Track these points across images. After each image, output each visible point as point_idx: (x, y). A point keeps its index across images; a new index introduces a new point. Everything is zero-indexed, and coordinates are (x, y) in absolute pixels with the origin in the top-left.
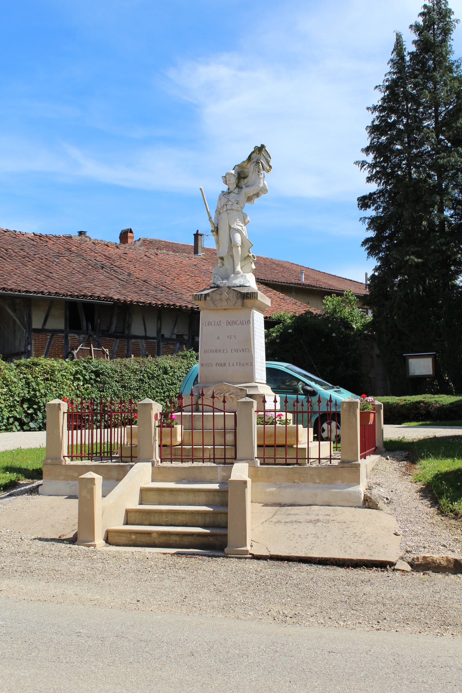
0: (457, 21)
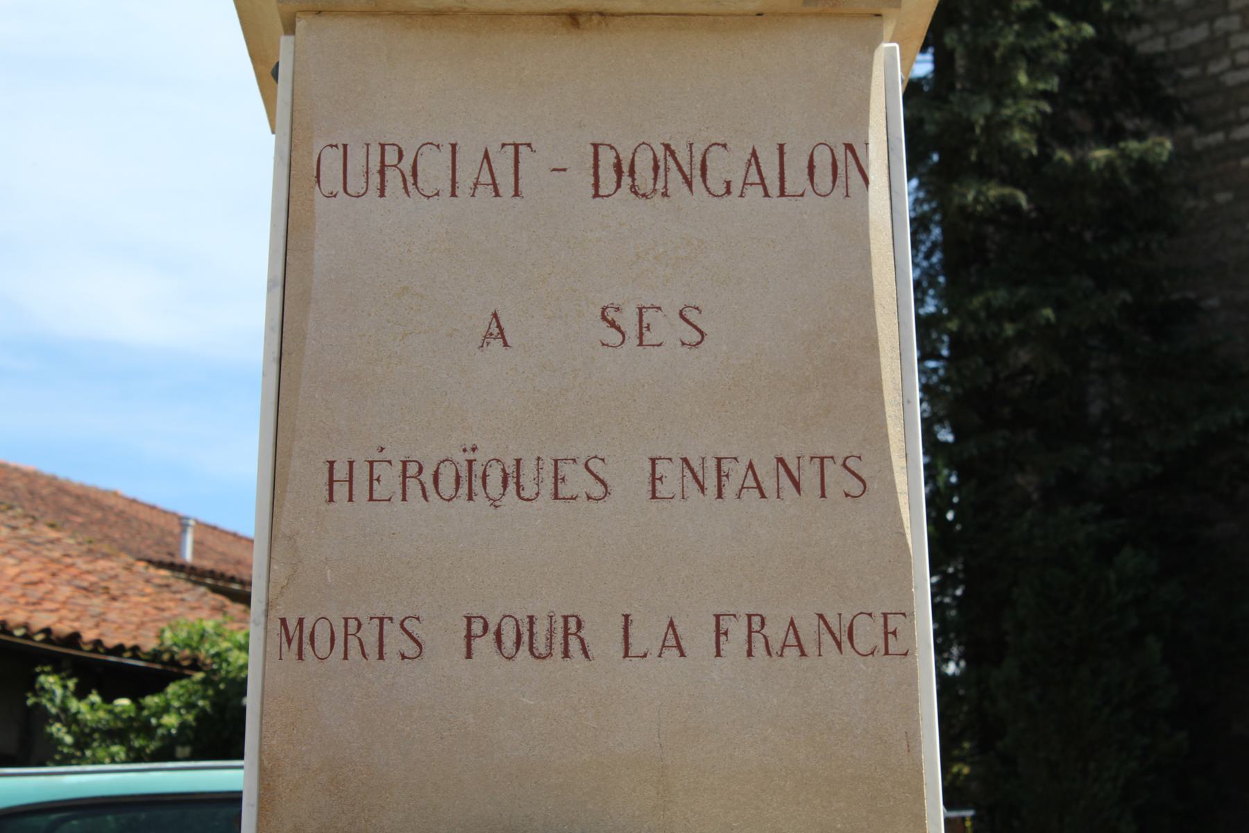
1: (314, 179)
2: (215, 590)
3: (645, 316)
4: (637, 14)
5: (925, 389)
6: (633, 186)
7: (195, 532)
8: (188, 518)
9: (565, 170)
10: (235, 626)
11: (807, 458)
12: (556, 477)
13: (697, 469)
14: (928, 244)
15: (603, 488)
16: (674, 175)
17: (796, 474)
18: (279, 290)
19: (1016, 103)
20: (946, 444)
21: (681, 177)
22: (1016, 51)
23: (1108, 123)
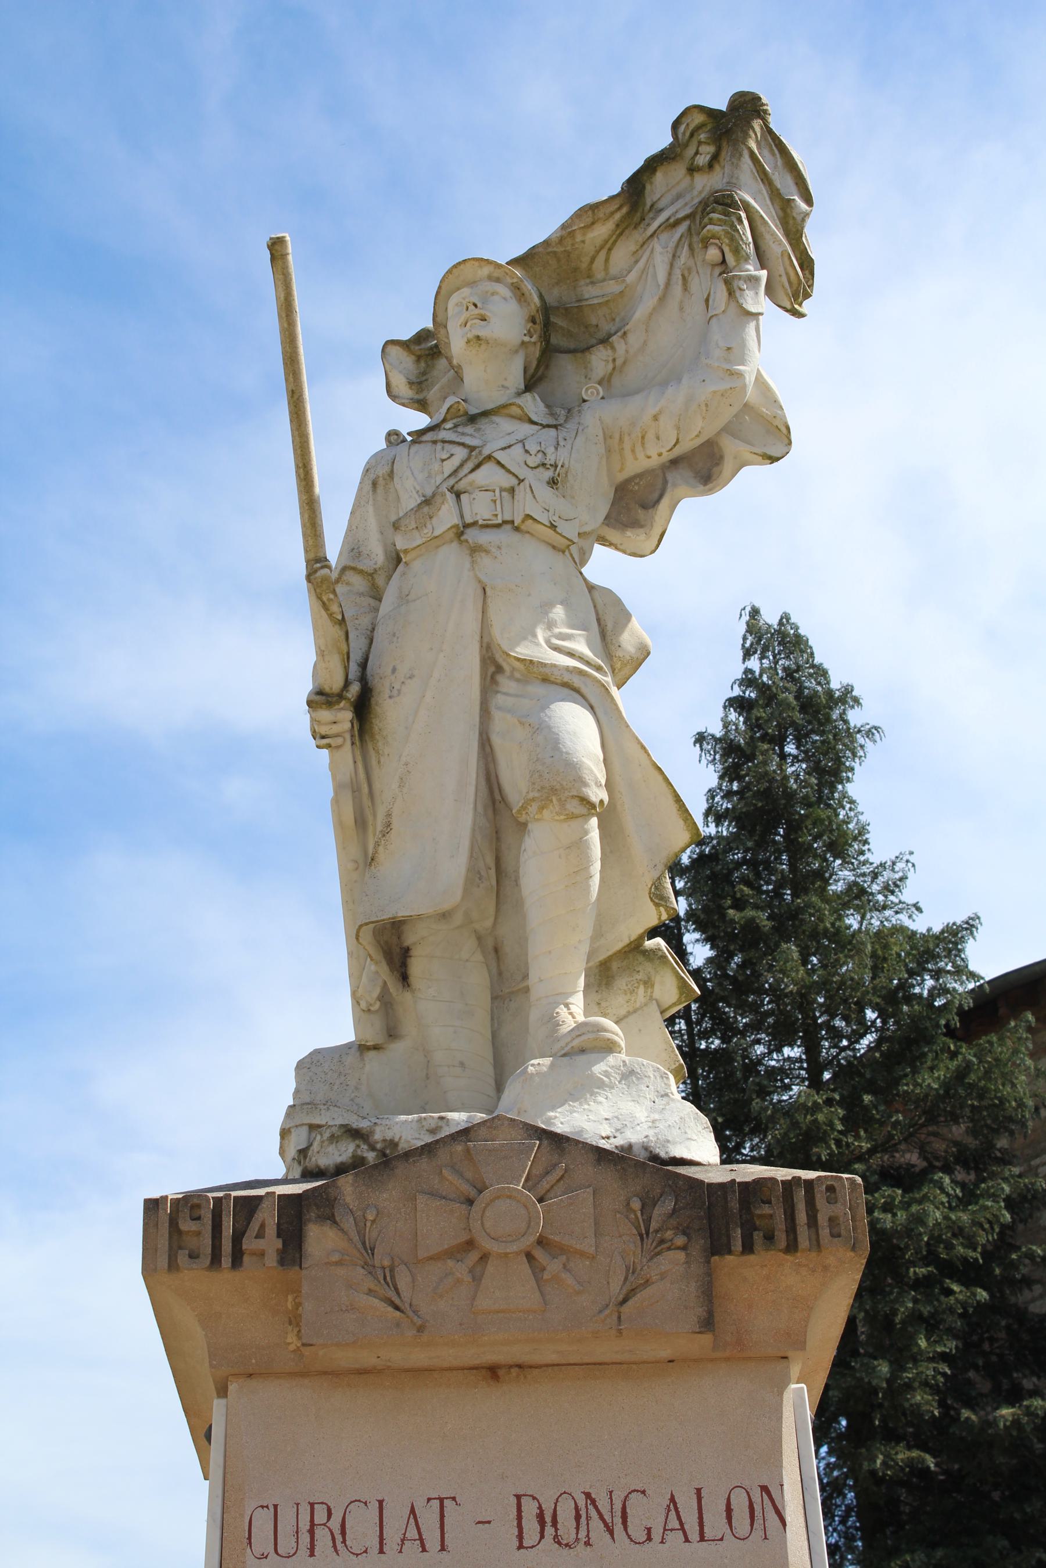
0: (871, 733)
1: (246, 1541)
4: (554, 1365)
6: (556, 1536)
9: (489, 1522)
16: (596, 1524)
19: (916, 1366)
21: (602, 1525)
22: (916, 1318)
23: (1006, 1384)
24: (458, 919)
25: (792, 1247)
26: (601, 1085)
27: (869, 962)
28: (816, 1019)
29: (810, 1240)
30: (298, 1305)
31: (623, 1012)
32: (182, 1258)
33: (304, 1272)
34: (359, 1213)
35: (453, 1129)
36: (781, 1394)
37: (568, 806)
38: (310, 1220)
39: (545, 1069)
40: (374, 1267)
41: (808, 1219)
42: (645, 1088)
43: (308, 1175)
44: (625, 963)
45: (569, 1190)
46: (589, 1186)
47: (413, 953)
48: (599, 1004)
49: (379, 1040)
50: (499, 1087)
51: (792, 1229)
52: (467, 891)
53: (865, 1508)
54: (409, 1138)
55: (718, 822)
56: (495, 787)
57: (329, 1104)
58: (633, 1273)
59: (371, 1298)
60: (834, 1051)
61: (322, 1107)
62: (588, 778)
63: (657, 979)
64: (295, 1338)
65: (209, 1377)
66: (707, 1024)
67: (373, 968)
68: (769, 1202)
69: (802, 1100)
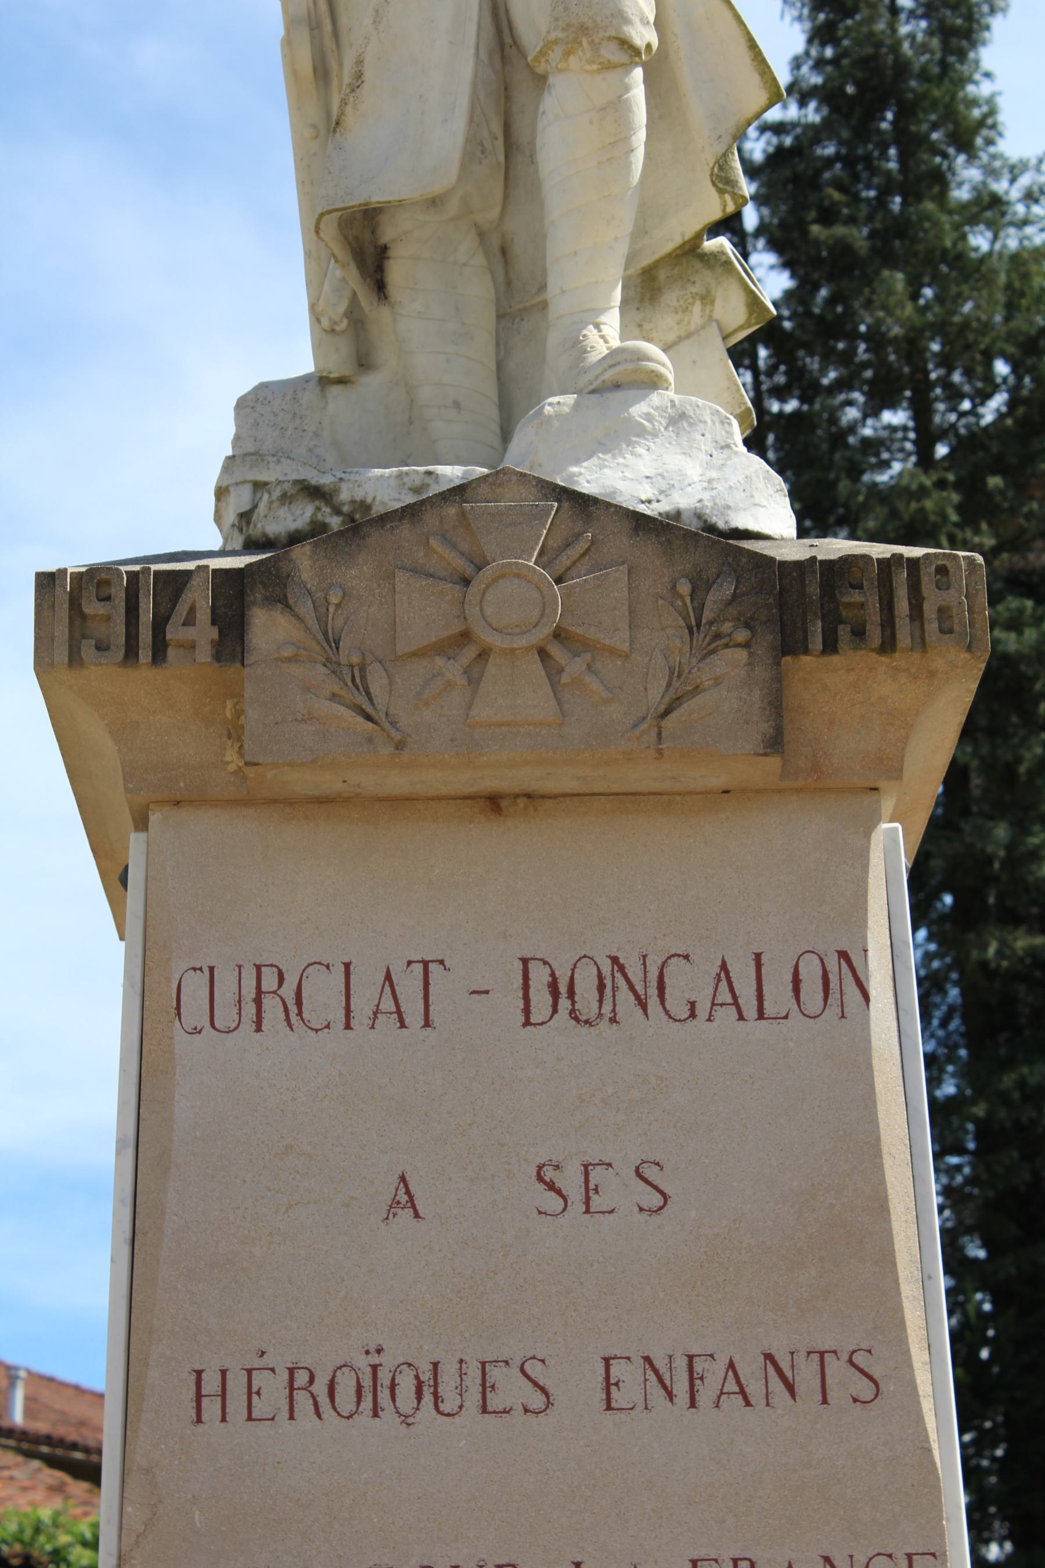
1: (173, 1011)
2: (53, 1462)
3: (592, 1175)
5: (946, 1192)
6: (573, 1011)
7: (27, 1383)
8: (17, 1368)
9: (487, 992)
10: (78, 1511)
11: (803, 1354)
12: (483, 1385)
13: (663, 1369)
14: (944, 1008)
15: (544, 1398)
16: (625, 996)
17: (789, 1374)
18: (130, 1152)
20: (976, 1261)
21: (633, 998)
24: (453, 207)
25: (888, 646)
26: (642, 432)
27: (1001, 298)
28: (927, 373)
29: (912, 636)
30: (239, 713)
31: (672, 337)
32: (87, 649)
33: (247, 670)
34: (320, 594)
35: (444, 487)
36: (867, 835)
37: (603, 52)
38: (254, 603)
39: (567, 410)
40: (339, 664)
41: (911, 610)
42: (699, 437)
43: (251, 546)
44: (676, 271)
45: (597, 567)
46: (623, 563)
47: (392, 253)
48: (640, 326)
49: (345, 371)
50: (506, 436)
51: (888, 622)
52: (464, 168)
53: (972, 1008)
54: (386, 499)
55: (802, 103)
56: (505, 24)
57: (280, 455)
58: (679, 676)
59: (335, 705)
60: (953, 417)
61: (270, 459)
62: (630, 12)
63: (719, 294)
64: (235, 756)
65: (126, 804)
66: (780, 379)
67: (338, 273)
68: (860, 587)
69: (905, 481)
